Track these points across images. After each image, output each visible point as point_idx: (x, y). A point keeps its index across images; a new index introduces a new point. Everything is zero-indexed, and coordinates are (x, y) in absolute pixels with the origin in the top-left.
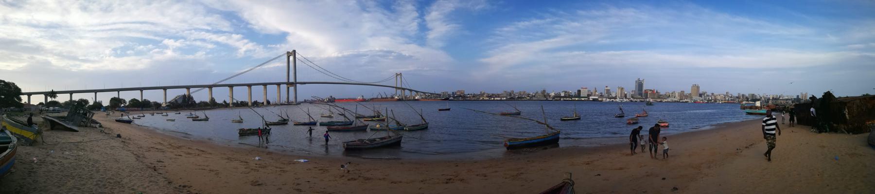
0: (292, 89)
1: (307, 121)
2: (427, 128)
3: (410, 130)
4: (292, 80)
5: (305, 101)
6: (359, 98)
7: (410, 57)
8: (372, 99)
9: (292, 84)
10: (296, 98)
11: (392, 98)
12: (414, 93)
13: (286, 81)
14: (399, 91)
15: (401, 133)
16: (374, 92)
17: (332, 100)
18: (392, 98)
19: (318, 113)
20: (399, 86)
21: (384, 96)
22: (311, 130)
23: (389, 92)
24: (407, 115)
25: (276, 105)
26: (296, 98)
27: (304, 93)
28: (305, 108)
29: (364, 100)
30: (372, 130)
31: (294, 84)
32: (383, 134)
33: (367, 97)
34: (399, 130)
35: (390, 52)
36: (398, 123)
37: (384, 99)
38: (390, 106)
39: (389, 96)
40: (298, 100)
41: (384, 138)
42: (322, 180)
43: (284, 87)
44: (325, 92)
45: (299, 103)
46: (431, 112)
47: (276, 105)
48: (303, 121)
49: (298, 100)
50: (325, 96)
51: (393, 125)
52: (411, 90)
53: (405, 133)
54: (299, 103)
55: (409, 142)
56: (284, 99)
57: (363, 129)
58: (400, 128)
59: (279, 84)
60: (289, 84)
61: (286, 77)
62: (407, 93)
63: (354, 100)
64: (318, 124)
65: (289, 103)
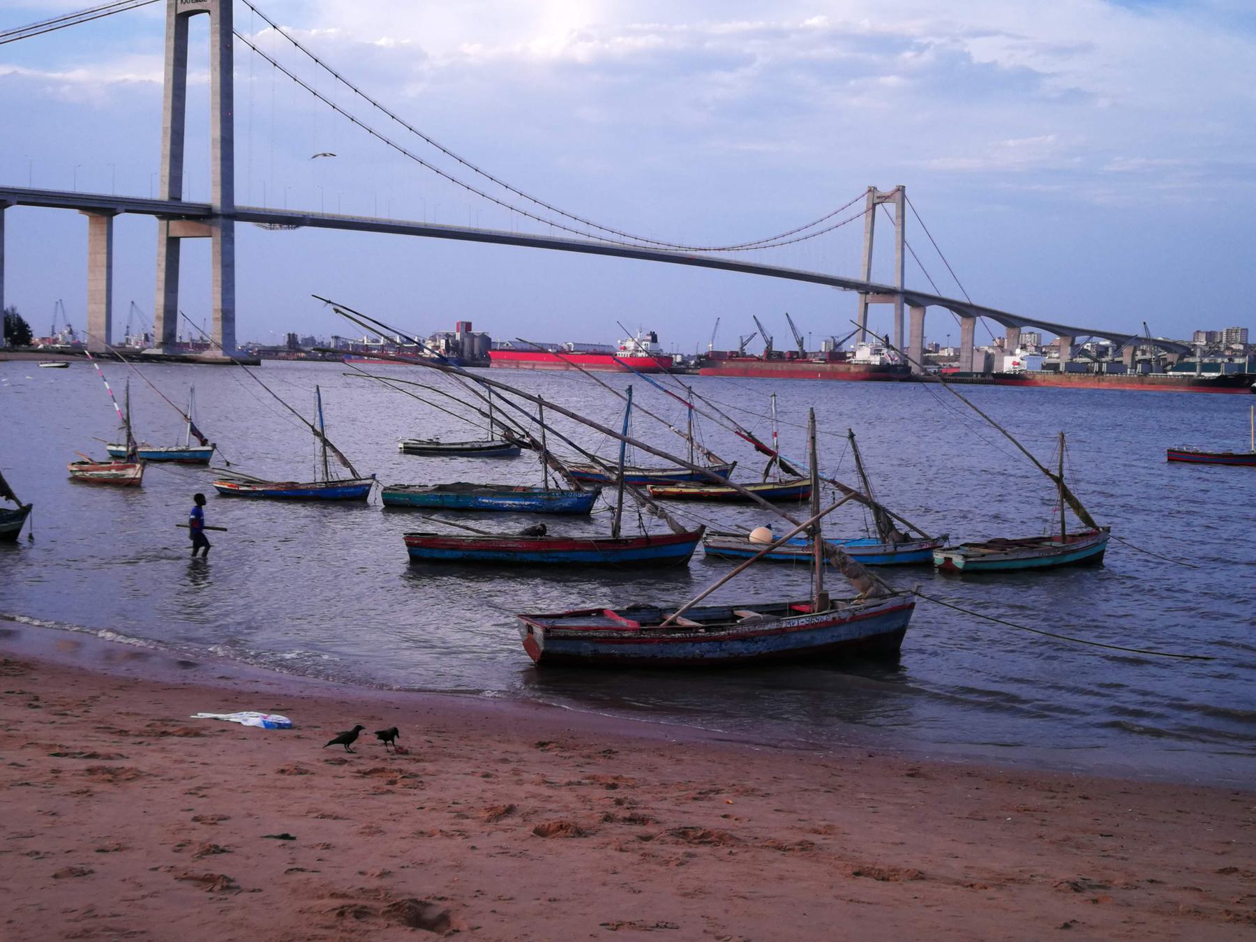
0: (198, 252)
1: (307, 475)
2: (1094, 562)
3: (976, 573)
4: (201, 188)
5: (294, 348)
6: (629, 346)
7: (1025, 80)
8: (710, 363)
9: (201, 216)
10: (228, 317)
11: (836, 356)
12: (988, 332)
13: (160, 192)
14: (883, 315)
15: (905, 583)
16: (696, 315)
17: (466, 354)
18: (836, 356)
19: (382, 426)
20: (885, 276)
21: (785, 344)
22: (294, 860)
23: (822, 318)
24: (947, 474)
25: (72, 353)
26: (228, 317)
27: (282, 285)
28: (296, 384)
29: (657, 365)
30: (716, 557)
31: (220, 219)
32: (797, 587)
33: (678, 346)
34: (892, 566)
35: (889, 45)
36: (883, 517)
37: (784, 364)
38: (840, 408)
39: (817, 345)
40: (244, 336)
41: (792, 609)
42: (372, 831)
43: (140, 236)
44: (427, 293)
45: (251, 359)
46: (1119, 463)
47: (72, 353)
48: (276, 474)
49: (244, 336)
50: (431, 325)
51: (847, 526)
52: (966, 311)
53: (937, 586)
54: (251, 359)
55: (944, 637)
56: (139, 319)
57: (663, 559)
58: (906, 556)
59: (102, 209)
60: (175, 211)
61: (162, 169)
62: (941, 329)
63: (601, 356)
64: (375, 497)
65: (174, 353)
